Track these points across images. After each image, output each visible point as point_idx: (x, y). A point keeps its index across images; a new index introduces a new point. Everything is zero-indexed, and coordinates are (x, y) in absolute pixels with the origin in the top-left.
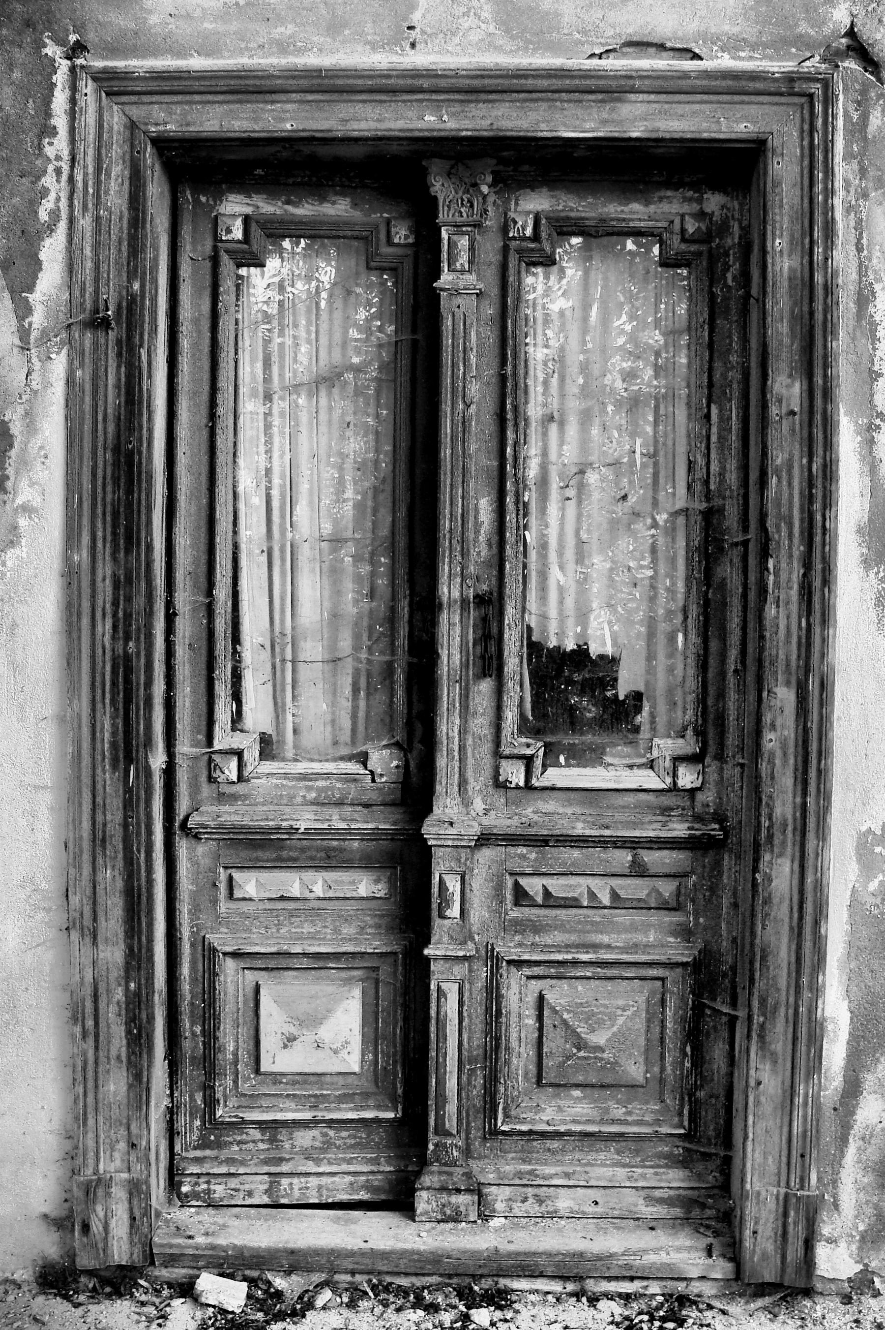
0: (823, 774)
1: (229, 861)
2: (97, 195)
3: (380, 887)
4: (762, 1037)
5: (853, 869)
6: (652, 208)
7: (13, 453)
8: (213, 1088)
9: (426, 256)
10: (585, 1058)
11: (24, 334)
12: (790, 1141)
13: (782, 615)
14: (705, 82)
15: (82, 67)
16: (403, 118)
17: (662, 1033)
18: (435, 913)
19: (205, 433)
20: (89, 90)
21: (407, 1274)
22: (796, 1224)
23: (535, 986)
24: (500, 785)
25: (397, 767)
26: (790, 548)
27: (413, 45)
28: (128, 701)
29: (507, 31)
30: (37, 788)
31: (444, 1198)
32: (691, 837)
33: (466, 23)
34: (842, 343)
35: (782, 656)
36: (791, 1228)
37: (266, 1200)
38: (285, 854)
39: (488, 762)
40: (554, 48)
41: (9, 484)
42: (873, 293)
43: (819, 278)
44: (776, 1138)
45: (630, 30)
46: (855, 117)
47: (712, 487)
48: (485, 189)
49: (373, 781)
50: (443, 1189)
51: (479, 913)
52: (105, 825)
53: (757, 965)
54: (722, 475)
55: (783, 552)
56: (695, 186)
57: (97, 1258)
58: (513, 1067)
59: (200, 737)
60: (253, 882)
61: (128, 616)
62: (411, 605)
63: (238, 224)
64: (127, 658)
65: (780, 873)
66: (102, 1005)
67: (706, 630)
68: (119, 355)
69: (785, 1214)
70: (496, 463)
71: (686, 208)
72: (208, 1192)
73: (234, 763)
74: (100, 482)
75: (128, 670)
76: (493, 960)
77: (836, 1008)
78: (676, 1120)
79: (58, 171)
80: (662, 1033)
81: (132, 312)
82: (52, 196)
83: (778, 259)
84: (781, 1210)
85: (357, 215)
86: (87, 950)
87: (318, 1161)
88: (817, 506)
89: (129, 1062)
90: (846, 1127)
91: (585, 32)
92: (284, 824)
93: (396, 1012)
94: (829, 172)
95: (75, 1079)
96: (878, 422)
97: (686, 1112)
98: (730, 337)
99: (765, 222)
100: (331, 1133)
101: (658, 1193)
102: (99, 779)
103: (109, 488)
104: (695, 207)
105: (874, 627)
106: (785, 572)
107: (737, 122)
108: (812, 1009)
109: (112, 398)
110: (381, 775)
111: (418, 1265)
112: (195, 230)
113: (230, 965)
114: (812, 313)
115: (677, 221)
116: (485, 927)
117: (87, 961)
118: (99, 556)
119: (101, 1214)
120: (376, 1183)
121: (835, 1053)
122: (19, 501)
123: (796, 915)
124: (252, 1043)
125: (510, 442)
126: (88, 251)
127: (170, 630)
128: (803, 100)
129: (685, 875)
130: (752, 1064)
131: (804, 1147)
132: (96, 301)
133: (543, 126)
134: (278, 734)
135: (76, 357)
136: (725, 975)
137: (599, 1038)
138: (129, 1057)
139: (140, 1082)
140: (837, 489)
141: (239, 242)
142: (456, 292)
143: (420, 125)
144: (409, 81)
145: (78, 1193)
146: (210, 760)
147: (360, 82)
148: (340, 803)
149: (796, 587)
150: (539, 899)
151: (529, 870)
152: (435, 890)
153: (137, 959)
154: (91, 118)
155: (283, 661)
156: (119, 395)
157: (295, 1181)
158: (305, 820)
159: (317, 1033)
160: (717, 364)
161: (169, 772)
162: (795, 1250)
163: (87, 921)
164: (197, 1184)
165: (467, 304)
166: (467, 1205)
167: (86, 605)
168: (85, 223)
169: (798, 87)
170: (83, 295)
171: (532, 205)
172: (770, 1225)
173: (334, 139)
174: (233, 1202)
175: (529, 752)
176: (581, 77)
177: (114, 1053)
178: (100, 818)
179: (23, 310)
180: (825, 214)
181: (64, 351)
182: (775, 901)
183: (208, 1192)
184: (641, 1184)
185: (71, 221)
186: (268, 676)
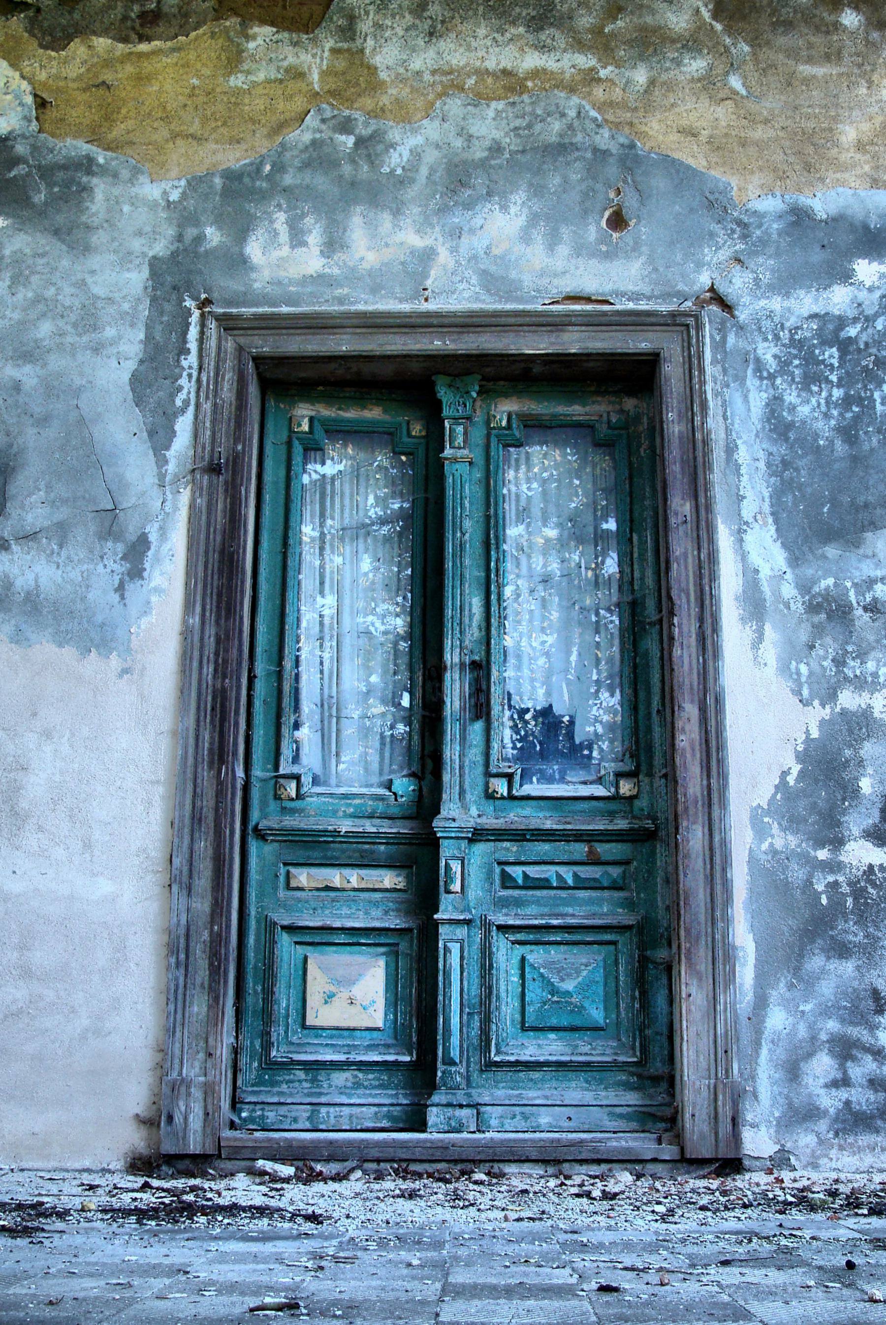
0: (721, 762)
1: (289, 858)
2: (216, 391)
3: (400, 879)
4: (689, 959)
5: (749, 835)
6: (588, 408)
7: (150, 553)
8: (269, 1034)
9: (436, 438)
10: (558, 1002)
11: (162, 476)
12: (715, 1041)
13: (685, 654)
14: (617, 318)
15: (209, 312)
16: (419, 342)
17: (617, 986)
18: (442, 889)
19: (279, 558)
20: (213, 326)
21: (422, 1161)
22: (724, 1105)
23: (520, 950)
24: (490, 796)
25: (414, 790)
26: (689, 609)
27: (426, 300)
28: (223, 720)
29: (488, 291)
30: (152, 782)
31: (450, 1111)
32: (631, 829)
33: (461, 287)
34: (716, 476)
35: (687, 682)
36: (720, 1110)
37: (308, 1125)
38: (329, 854)
39: (480, 780)
40: (519, 300)
41: (145, 574)
42: (737, 446)
43: (698, 436)
44: (705, 1039)
45: (568, 290)
46: (718, 338)
47: (636, 588)
48: (474, 395)
49: (396, 800)
50: (449, 1105)
51: (475, 892)
52: (202, 808)
53: (682, 903)
54: (642, 579)
55: (684, 613)
56: (616, 393)
57: (177, 1145)
58: (503, 1014)
59: (269, 766)
60: (305, 875)
61: (225, 661)
62: (424, 675)
63: (306, 420)
64: (224, 690)
65: (694, 838)
66: (192, 944)
67: (636, 685)
68: (226, 491)
69: (716, 1100)
70: (483, 574)
71: (610, 408)
72: (263, 1117)
73: (293, 784)
74: (210, 572)
75: (224, 699)
76: (486, 925)
77: (743, 936)
78: (631, 1052)
79: (190, 376)
80: (617, 986)
81: (236, 462)
82: (185, 391)
83: (670, 425)
84: (712, 1097)
85: (386, 418)
86: (183, 900)
87: (349, 1096)
88: (706, 580)
89: (210, 987)
90: (758, 1032)
91: (538, 291)
92: (330, 828)
93: (411, 977)
94: (702, 371)
95: (168, 999)
96: (745, 527)
97: (637, 1044)
98: (644, 489)
99: (661, 403)
100: (360, 1075)
101: (618, 1110)
102: (199, 775)
103: (216, 577)
104: (618, 407)
105: (752, 663)
106: (685, 625)
107: (640, 342)
108: (725, 935)
109: (220, 519)
110: (402, 796)
111: (431, 1151)
112: (276, 426)
113: (285, 940)
114: (695, 458)
115: (605, 415)
116: (480, 903)
117: (183, 908)
118: (208, 622)
119: (183, 1108)
120: (395, 1113)
121: (746, 974)
122: (152, 585)
123: (709, 867)
124: (300, 1004)
125: (493, 559)
126: (208, 424)
127: (250, 688)
128: (683, 328)
129: (627, 863)
130: (683, 980)
131: (727, 1044)
132: (212, 457)
133: (512, 347)
134: (324, 774)
135: (197, 490)
136: (662, 936)
137: (569, 985)
138: (210, 985)
139: (218, 1004)
140: (719, 570)
141: (306, 433)
142: (455, 460)
143: (431, 347)
144: (424, 320)
145: (166, 1089)
146: (276, 782)
147: (391, 320)
148: (371, 817)
149: (694, 636)
150: (520, 881)
151: (512, 859)
152: (442, 871)
153: (219, 908)
154: (213, 343)
155: (331, 716)
156: (225, 517)
157: (332, 1109)
158: (346, 826)
159: (353, 995)
160: (636, 507)
161: (246, 788)
162: (725, 1127)
163: (185, 879)
164: (254, 1110)
165: (462, 469)
166: (468, 1118)
167: (196, 654)
168: (207, 406)
169: (679, 320)
170: (203, 452)
171: (505, 409)
172: (705, 1111)
173: (373, 357)
174: (282, 1127)
175: (510, 771)
176: (536, 316)
177: (198, 981)
178: (198, 803)
179: (162, 461)
180: (701, 396)
181: (189, 488)
182: (693, 856)
183: (263, 1117)
184: (604, 1102)
185: (198, 406)
186: (319, 726)
